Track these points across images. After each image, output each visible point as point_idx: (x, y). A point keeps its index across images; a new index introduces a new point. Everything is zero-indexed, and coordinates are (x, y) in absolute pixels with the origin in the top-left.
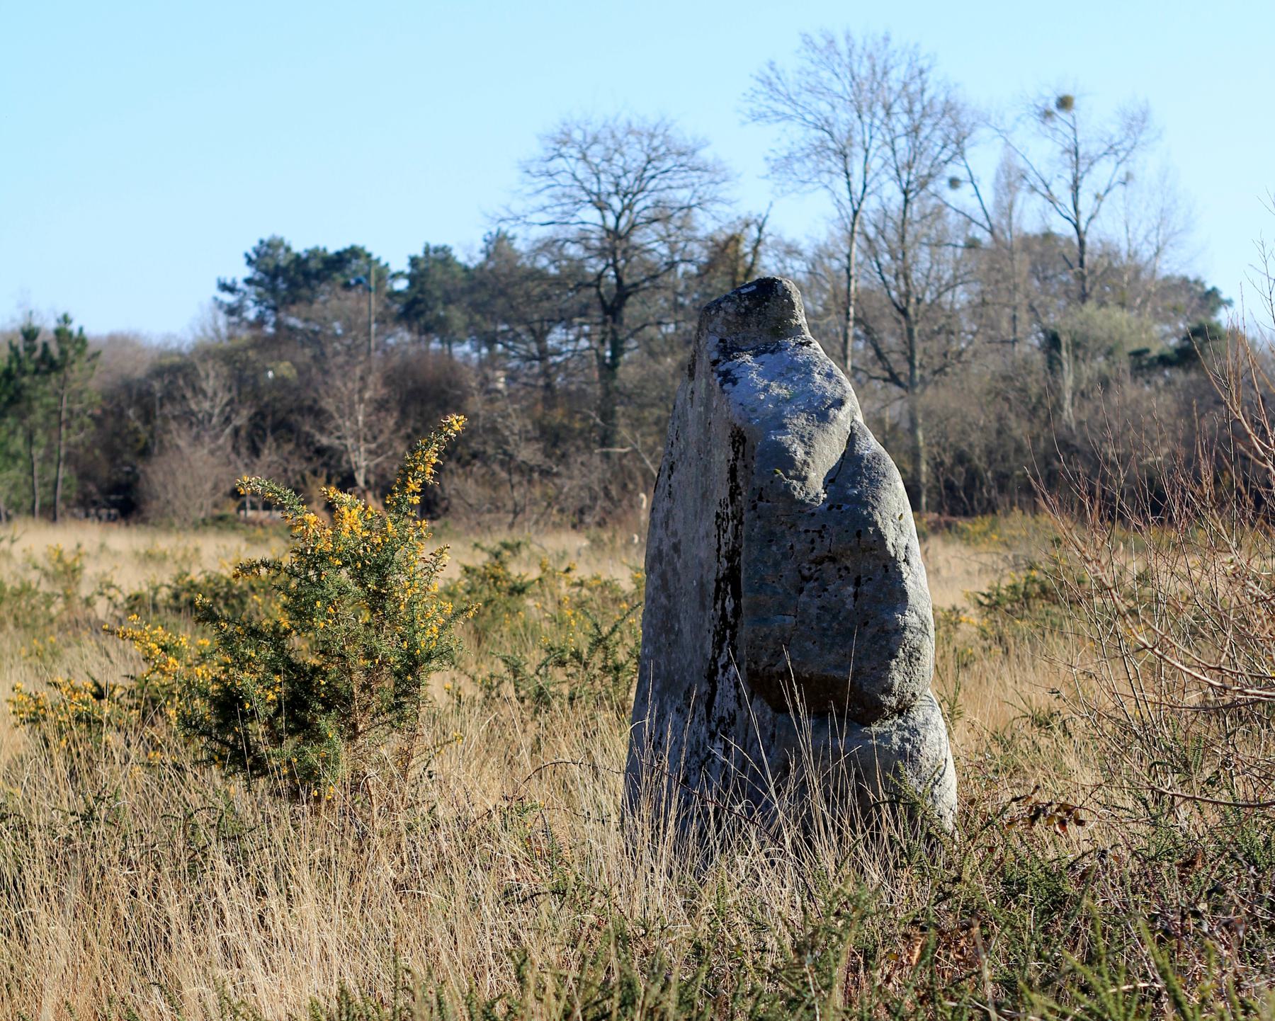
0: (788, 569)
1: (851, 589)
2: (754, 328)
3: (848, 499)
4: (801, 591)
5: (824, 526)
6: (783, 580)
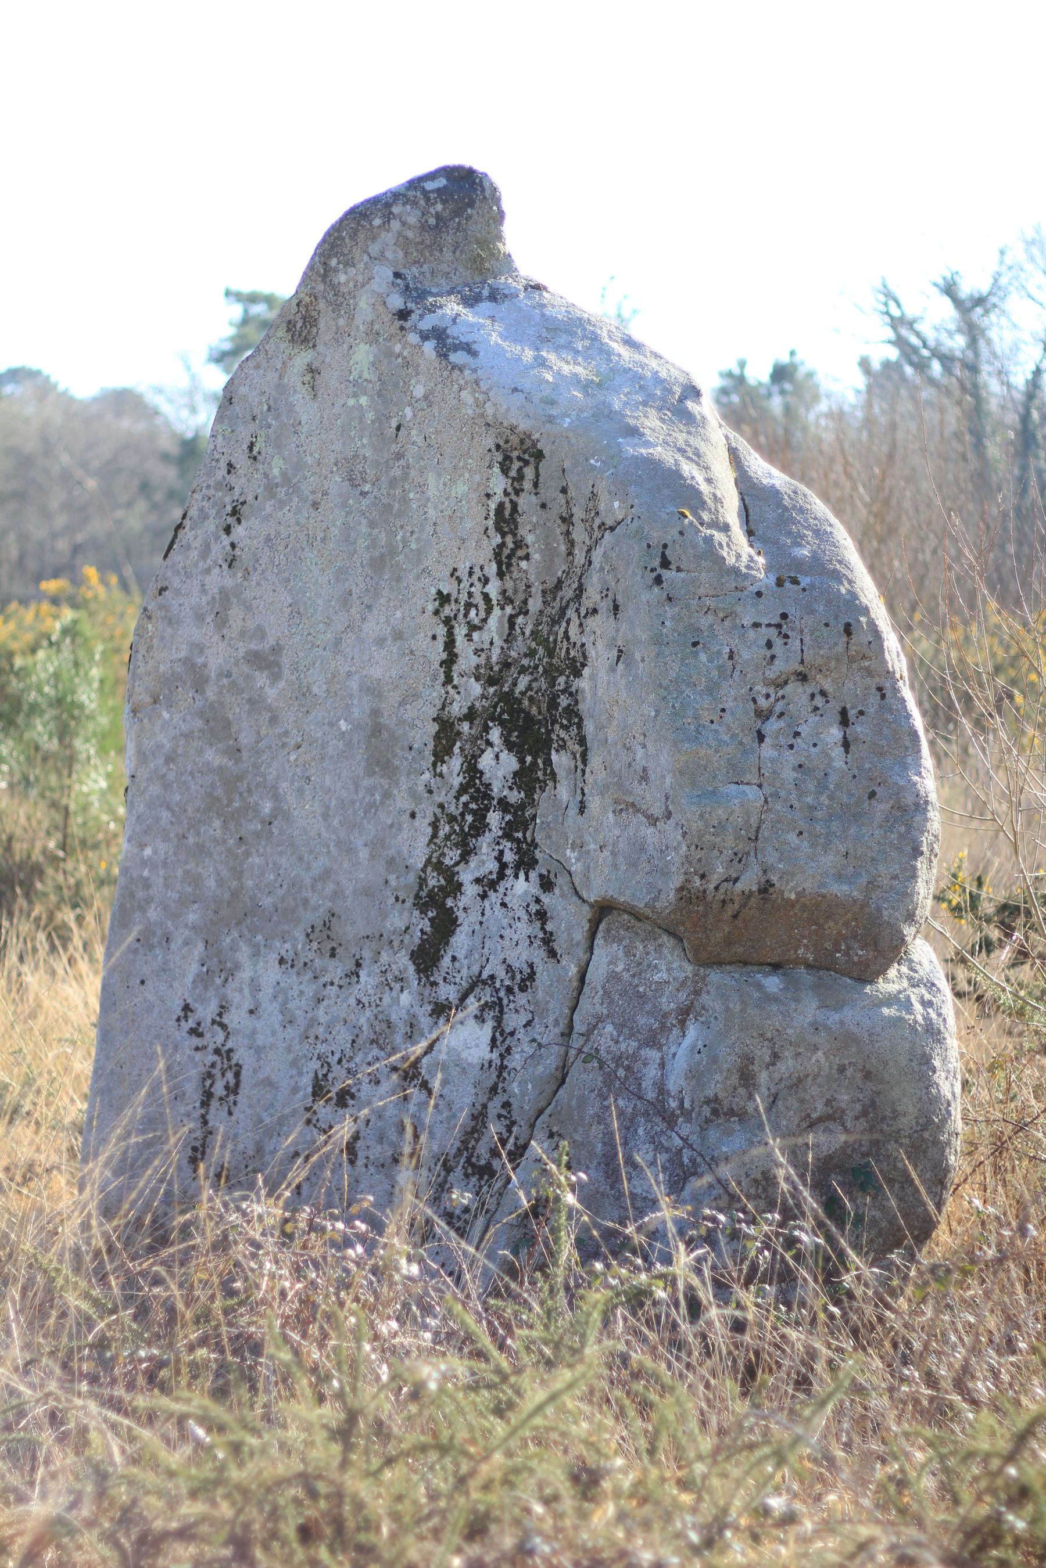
0: (730, 694)
1: (835, 733)
2: (448, 255)
3: (798, 564)
4: (761, 737)
5: (784, 616)
6: (728, 717)
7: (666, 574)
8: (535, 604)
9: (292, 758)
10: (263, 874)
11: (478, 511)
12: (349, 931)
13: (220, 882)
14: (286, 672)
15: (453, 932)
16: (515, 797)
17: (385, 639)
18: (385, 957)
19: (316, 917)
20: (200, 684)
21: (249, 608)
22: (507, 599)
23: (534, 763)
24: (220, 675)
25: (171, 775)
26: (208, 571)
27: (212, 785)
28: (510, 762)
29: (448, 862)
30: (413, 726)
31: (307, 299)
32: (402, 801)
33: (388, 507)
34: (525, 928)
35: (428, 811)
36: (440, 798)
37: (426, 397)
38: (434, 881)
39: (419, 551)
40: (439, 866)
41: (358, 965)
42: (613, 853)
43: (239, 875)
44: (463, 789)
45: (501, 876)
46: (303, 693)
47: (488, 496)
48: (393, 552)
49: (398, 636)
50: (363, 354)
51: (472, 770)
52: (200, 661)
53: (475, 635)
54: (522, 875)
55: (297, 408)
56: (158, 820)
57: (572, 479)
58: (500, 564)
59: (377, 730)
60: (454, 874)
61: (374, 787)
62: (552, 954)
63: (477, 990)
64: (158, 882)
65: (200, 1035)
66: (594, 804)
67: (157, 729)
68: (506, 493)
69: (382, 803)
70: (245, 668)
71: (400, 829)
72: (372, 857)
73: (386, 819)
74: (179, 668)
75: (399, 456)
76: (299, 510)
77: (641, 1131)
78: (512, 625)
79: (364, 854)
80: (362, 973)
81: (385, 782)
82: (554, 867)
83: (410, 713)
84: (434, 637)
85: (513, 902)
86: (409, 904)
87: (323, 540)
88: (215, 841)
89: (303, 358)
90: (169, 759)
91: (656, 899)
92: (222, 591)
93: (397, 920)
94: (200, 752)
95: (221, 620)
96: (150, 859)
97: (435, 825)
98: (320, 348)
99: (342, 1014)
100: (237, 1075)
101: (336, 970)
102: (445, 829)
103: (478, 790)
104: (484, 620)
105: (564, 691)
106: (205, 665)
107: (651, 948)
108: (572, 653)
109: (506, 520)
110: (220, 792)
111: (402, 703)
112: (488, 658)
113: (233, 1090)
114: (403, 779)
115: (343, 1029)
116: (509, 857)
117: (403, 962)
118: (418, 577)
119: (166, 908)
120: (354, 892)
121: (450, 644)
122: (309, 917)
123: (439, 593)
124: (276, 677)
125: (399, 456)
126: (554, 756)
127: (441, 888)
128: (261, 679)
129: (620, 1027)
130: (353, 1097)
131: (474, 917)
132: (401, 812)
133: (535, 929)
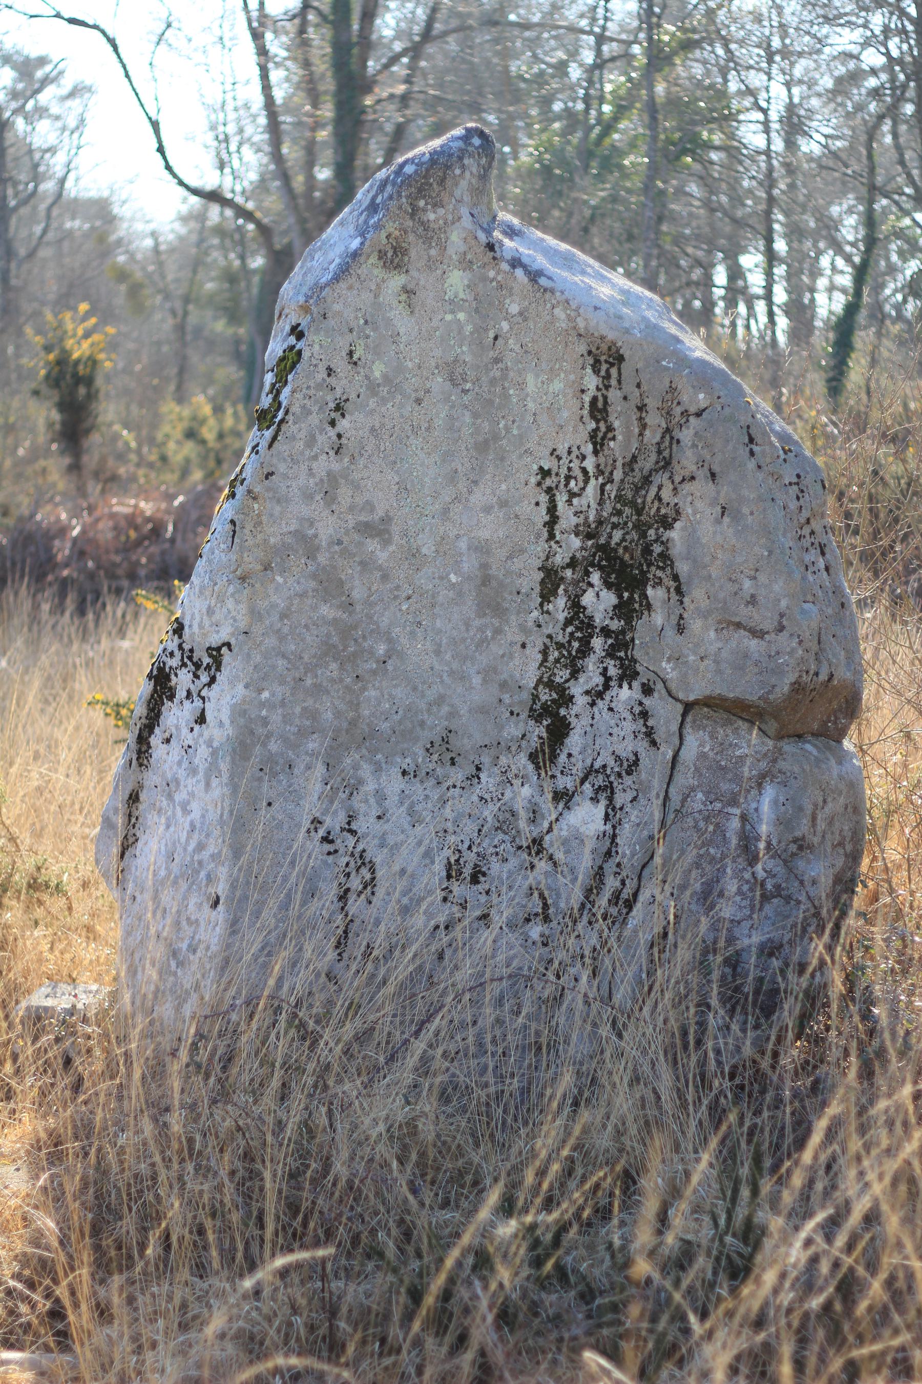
8: (618, 475)
9: (404, 608)
10: (379, 704)
11: (574, 404)
12: (462, 743)
13: (338, 714)
14: (396, 538)
15: (567, 734)
16: (615, 625)
17: (492, 507)
18: (503, 761)
19: (436, 734)
20: (311, 553)
21: (357, 487)
22: (600, 472)
23: (631, 598)
24: (331, 544)
25: (286, 630)
26: (315, 458)
27: (328, 635)
28: (610, 598)
29: (558, 679)
30: (520, 575)
31: (397, 233)
32: (512, 634)
33: (490, 402)
34: (629, 726)
35: (537, 641)
36: (549, 631)
37: (521, 314)
38: (545, 696)
39: (521, 436)
40: (550, 685)
41: (478, 769)
42: (717, 662)
43: (355, 706)
44: (568, 622)
45: (607, 687)
46: (414, 554)
47: (583, 391)
48: (496, 437)
49: (503, 504)
50: (457, 280)
51: (576, 605)
52: (311, 532)
53: (575, 501)
54: (625, 685)
55: (395, 322)
56: (274, 667)
57: (644, 377)
58: (595, 444)
59: (486, 580)
60: (565, 689)
61: (486, 626)
62: (654, 743)
63: (591, 778)
64: (276, 718)
65: (331, 842)
66: (695, 625)
67: (271, 591)
68: (598, 389)
69: (493, 638)
70: (356, 537)
71: (511, 657)
72: (485, 681)
73: (497, 649)
74: (289, 540)
75: (497, 360)
76: (402, 406)
77: (729, 870)
78: (602, 491)
79: (476, 680)
80: (482, 775)
81: (496, 622)
82: (652, 676)
83: (517, 564)
84: (537, 504)
85: (619, 706)
86: (524, 716)
87: (428, 429)
88: (333, 681)
89: (397, 281)
90: (283, 616)
91: (769, 693)
92: (329, 473)
93: (513, 730)
94: (315, 608)
95: (329, 496)
96: (267, 700)
97: (545, 652)
98: (413, 273)
99: (463, 812)
100: (373, 871)
101: (457, 775)
102: (554, 655)
103: (582, 622)
104: (583, 489)
105: (656, 541)
106: (316, 536)
107: (729, 731)
108: (663, 511)
109: (598, 410)
110: (335, 639)
111: (510, 557)
112: (587, 518)
113: (370, 884)
114: (513, 617)
115: (469, 822)
116: (613, 672)
117: (522, 762)
118: (520, 457)
119: (286, 740)
120: (470, 711)
121: (552, 509)
122: (426, 736)
123: (541, 468)
124: (386, 542)
125: (497, 360)
126: (650, 592)
127: (553, 701)
128: (372, 545)
129: (707, 793)
130: (484, 874)
131: (585, 721)
132: (512, 644)
133: (639, 725)
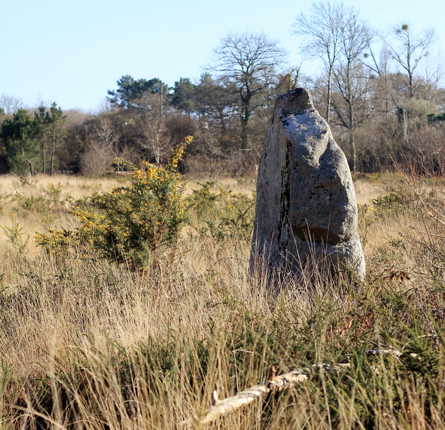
0: (306, 190)
2: (295, 106)
4: (311, 198)
7: (297, 167)
